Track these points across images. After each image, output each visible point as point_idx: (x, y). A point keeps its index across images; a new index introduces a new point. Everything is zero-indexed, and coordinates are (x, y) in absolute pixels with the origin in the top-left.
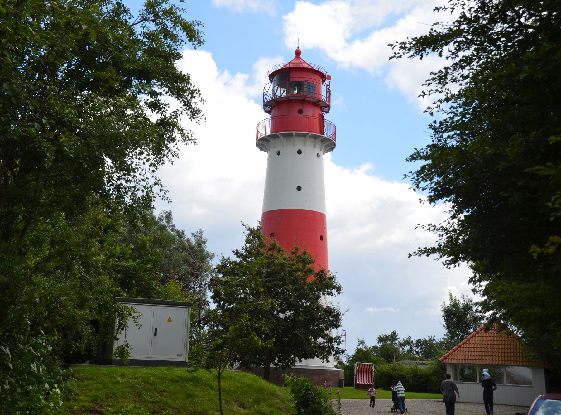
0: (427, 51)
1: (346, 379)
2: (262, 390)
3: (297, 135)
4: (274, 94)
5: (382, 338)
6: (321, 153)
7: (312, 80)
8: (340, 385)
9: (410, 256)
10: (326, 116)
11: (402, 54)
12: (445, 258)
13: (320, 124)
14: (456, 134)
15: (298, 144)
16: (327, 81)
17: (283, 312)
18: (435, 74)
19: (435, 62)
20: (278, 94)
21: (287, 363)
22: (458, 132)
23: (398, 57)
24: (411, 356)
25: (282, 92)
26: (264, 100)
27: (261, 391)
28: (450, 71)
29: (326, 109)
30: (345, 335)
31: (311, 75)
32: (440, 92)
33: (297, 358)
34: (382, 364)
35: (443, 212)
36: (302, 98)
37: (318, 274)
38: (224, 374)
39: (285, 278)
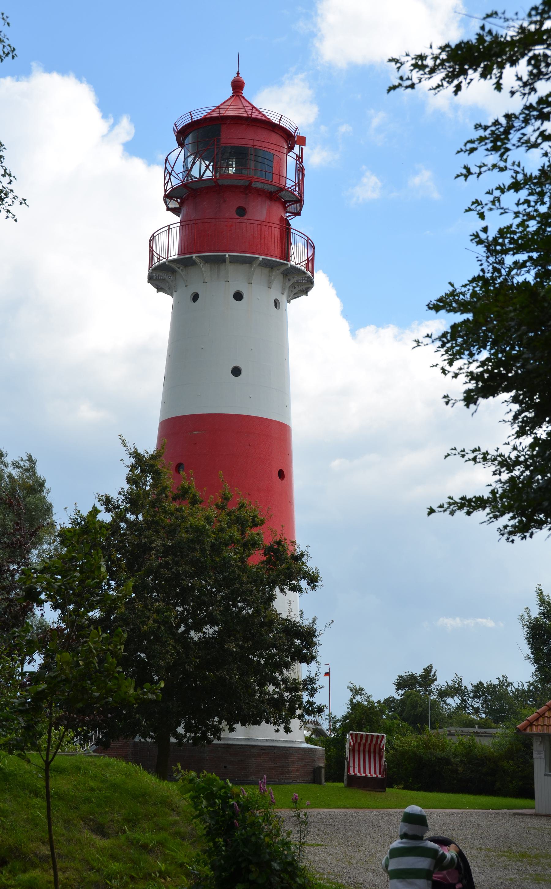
0: (469, 77)
1: (328, 766)
2: (144, 795)
3: (235, 260)
4: (188, 171)
5: (404, 681)
6: (283, 299)
7: (264, 144)
8: (316, 780)
9: (432, 511)
10: (294, 222)
11: (415, 80)
12: (506, 520)
13: (282, 239)
14: (530, 258)
15: (236, 278)
16: (297, 148)
17: (199, 629)
18: (486, 128)
19: (487, 97)
20: (195, 173)
21: (204, 734)
22: (535, 255)
23: (407, 87)
24: (465, 716)
25: (203, 170)
26: (166, 184)
27: (141, 796)
28: (517, 124)
29: (296, 207)
30: (327, 674)
31: (276, 138)
32: (502, 170)
33: (224, 723)
34: (404, 735)
35: (498, 421)
36: (242, 183)
37: (268, 551)
38: (59, 760)
39: (203, 559)
